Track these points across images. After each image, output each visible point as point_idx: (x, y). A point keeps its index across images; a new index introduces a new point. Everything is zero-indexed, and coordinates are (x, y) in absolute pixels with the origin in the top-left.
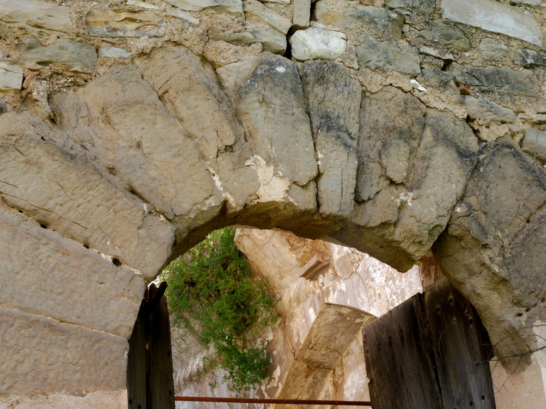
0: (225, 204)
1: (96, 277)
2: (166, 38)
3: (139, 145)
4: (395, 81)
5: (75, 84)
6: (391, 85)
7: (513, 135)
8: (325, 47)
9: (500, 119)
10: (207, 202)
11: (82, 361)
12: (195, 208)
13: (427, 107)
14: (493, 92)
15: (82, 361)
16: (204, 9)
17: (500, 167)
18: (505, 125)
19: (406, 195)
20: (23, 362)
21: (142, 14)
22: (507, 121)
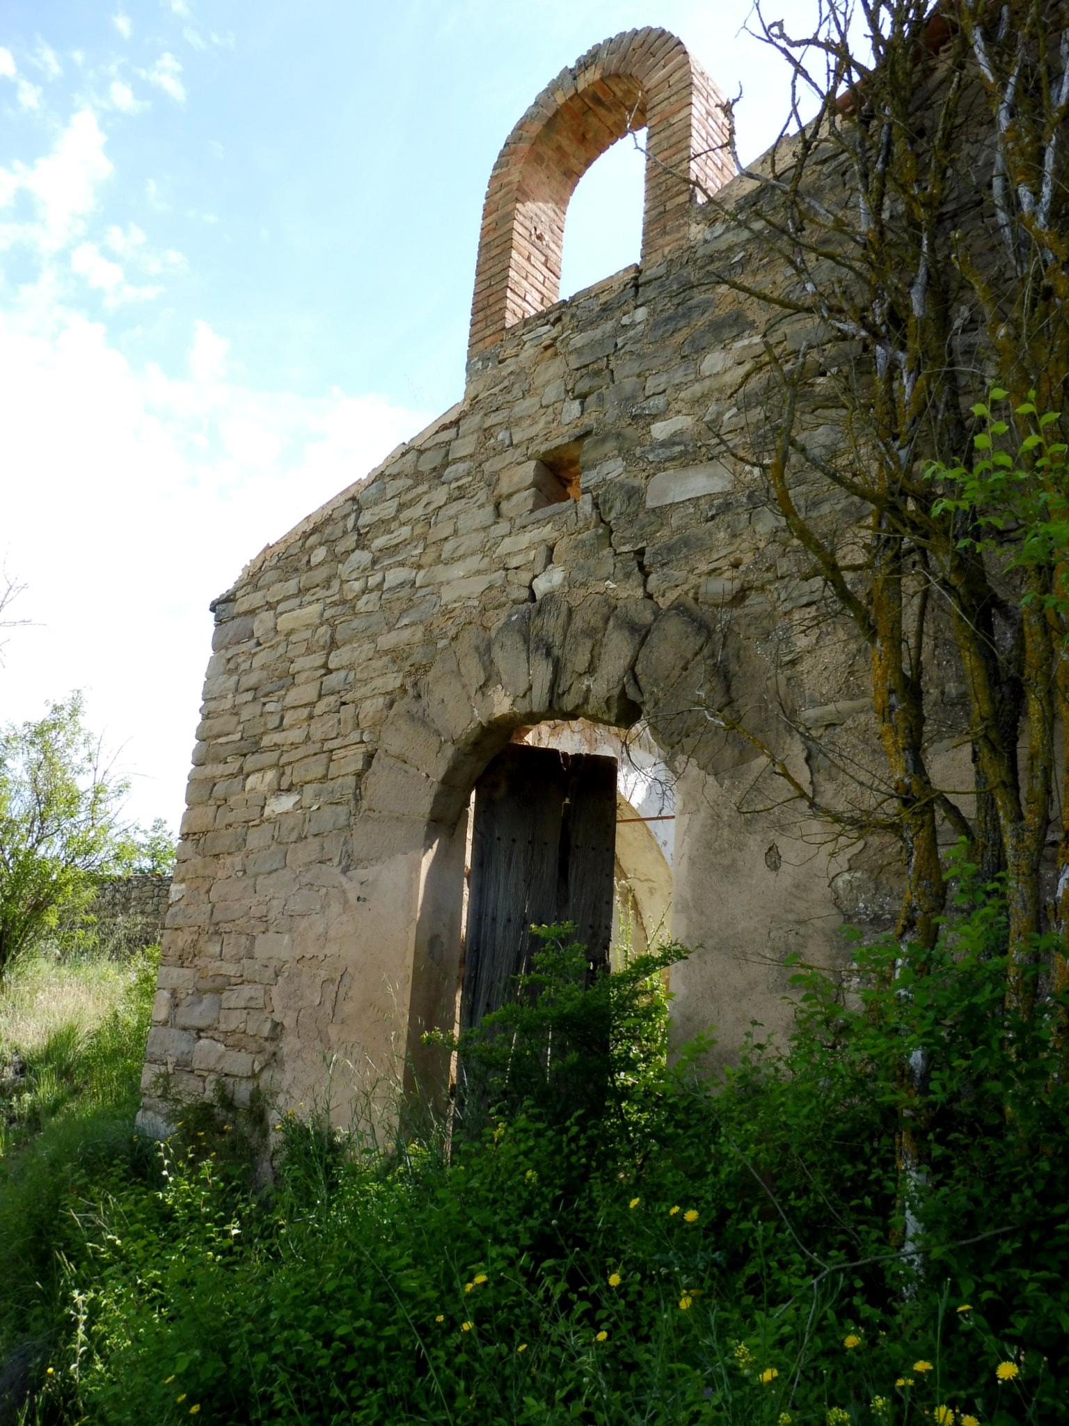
7: (686, 593)
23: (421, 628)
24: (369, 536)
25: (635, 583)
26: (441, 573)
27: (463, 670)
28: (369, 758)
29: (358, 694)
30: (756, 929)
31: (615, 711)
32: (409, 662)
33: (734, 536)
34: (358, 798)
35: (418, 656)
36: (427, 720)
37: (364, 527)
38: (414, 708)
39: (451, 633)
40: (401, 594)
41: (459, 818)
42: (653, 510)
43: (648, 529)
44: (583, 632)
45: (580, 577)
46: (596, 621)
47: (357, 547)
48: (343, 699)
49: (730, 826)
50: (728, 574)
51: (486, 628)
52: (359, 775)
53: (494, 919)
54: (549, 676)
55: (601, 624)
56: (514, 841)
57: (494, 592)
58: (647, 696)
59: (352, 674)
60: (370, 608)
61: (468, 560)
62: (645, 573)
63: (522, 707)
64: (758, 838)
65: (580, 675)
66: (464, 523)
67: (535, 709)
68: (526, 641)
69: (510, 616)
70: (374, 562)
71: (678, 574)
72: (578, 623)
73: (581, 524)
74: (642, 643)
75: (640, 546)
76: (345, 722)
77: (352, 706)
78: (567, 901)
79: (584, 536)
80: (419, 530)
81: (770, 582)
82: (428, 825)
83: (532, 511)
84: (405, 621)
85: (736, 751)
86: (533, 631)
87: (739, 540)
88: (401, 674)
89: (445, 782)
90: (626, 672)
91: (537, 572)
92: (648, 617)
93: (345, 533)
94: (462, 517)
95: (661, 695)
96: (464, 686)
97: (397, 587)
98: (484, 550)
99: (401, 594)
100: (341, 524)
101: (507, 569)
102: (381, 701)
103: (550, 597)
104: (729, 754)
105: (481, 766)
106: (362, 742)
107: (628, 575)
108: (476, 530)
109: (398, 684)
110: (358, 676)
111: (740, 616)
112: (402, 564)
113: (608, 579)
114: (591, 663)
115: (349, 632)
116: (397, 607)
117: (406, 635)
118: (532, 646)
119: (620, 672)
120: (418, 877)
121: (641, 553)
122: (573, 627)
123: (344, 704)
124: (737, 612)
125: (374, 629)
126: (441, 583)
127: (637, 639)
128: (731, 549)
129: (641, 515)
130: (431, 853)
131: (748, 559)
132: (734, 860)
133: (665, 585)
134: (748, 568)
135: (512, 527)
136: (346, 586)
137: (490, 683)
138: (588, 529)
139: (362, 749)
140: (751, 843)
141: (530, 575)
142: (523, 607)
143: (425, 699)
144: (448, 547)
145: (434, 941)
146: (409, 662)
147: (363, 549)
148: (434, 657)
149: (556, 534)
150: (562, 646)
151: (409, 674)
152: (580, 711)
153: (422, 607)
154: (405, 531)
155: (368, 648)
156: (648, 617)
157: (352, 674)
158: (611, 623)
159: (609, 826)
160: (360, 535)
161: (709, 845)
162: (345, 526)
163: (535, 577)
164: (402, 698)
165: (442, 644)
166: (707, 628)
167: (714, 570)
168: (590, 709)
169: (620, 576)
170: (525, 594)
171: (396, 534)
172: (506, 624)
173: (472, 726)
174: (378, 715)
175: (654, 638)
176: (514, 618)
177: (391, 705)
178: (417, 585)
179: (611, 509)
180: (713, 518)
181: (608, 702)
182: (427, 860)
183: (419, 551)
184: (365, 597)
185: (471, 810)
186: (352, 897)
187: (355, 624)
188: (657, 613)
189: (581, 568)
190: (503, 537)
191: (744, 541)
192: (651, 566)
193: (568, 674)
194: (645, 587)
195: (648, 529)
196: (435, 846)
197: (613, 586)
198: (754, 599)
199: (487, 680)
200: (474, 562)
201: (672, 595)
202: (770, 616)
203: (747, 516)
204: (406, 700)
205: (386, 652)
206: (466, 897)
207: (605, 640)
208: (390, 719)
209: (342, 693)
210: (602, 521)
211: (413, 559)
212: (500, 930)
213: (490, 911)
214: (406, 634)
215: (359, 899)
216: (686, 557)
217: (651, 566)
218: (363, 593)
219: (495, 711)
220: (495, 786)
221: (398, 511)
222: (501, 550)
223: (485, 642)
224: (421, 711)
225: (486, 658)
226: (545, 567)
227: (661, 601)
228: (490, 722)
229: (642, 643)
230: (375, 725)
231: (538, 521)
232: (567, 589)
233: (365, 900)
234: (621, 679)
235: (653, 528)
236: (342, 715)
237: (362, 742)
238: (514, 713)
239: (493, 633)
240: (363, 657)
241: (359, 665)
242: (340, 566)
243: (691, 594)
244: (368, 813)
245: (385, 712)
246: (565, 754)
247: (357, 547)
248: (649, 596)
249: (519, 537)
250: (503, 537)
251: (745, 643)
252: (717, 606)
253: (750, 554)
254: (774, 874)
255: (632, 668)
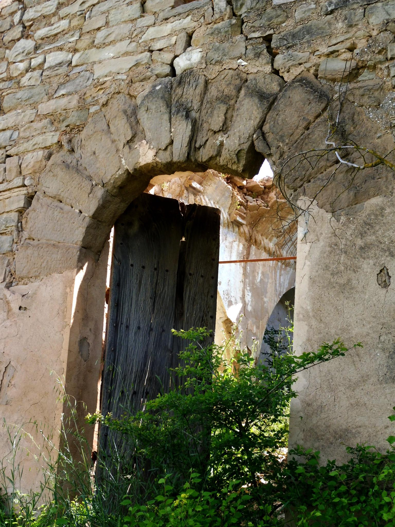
0: (127, 170)
1: (72, 221)
2: (113, 93)
3: (94, 153)
4: (227, 66)
5: (79, 131)
6: (225, 69)
7: (308, 70)
8: (188, 62)
9: (297, 63)
10: (117, 173)
11: (62, 259)
12: (113, 177)
13: (247, 74)
14: (296, 45)
15: (62, 259)
16: (130, 68)
17: (289, 97)
18: (302, 65)
19: (222, 137)
20: (44, 262)
21: (105, 84)
22: (303, 62)
23: (76, 97)
24: (32, 28)
25: (265, 61)
26: (94, 55)
27: (112, 129)
28: (30, 199)
29: (21, 148)
30: (368, 334)
31: (243, 162)
32: (65, 124)
33: (351, 26)
34: (20, 229)
35: (73, 119)
36: (80, 168)
37: (28, 21)
38: (69, 159)
39: (103, 100)
40: (59, 72)
41: (103, 247)
42: (280, 6)
43: (275, 21)
44: (217, 99)
45: (216, 57)
46: (230, 91)
47: (22, 37)
48: (8, 153)
49: (346, 252)
50: (344, 56)
51: (131, 96)
52: (21, 212)
53: (127, 327)
54: (188, 133)
55: (234, 93)
56: (143, 267)
57: (140, 68)
58: (273, 150)
59: (16, 134)
60: (32, 82)
61: (118, 45)
62: (273, 54)
63: (164, 158)
64: (371, 262)
65: (215, 132)
66: (113, 17)
67: (175, 159)
68: (169, 105)
69: (154, 86)
70: (36, 48)
71: (302, 55)
72: (213, 92)
73: (217, 16)
74: (269, 108)
75: (268, 33)
76: (10, 170)
77: (16, 158)
78: (182, 314)
79: (220, 25)
80: (75, 22)
81: (381, 62)
82: (80, 251)
83: (173, 7)
84: (62, 92)
85: (352, 193)
86: (174, 98)
87: (355, 29)
88: (58, 133)
89: (95, 217)
90: (255, 131)
91: (177, 53)
92: (275, 87)
93: (12, 26)
94: (113, 12)
95: (286, 148)
96: (113, 141)
97: (56, 66)
98: (131, 38)
99: (59, 72)
100: (9, 19)
101: (151, 51)
102: (40, 154)
103: (189, 72)
104: (345, 197)
105: (123, 206)
106: (24, 186)
107: (258, 55)
108: (125, 22)
109: (55, 140)
110: (21, 135)
111: (354, 88)
112: (60, 49)
113: (240, 58)
114: (225, 123)
115: (15, 101)
116: (55, 82)
117: (63, 102)
118: (173, 110)
119: (251, 130)
120: (72, 291)
121: (268, 39)
122: (208, 96)
123: (8, 156)
124: (352, 85)
125: (36, 98)
126: (95, 63)
127: (266, 104)
128: (348, 36)
129: (268, 10)
130: (82, 273)
131: (362, 44)
132: (349, 280)
133: (290, 63)
134: (362, 51)
135: (156, 19)
136: (12, 67)
137: (136, 139)
138: (223, 20)
139: (24, 191)
140: (365, 266)
141: (172, 56)
142: (167, 79)
143: (77, 155)
144: (100, 36)
145: (83, 341)
146: (65, 124)
147: (27, 38)
148: (86, 119)
149: (195, 24)
150: (200, 110)
151: (65, 133)
152: (212, 163)
153: (78, 81)
154: (64, 24)
155: (30, 113)
156: (275, 87)
157: (16, 134)
158: (243, 92)
159: (214, 260)
160: (24, 27)
161: (327, 267)
162: (12, 21)
163: (176, 57)
164: (58, 152)
165: (93, 109)
166: (326, 96)
167: (332, 53)
168: (222, 161)
169: (251, 55)
170: (167, 69)
171: (55, 26)
172: (151, 93)
173: (120, 172)
174: (37, 166)
175: (280, 104)
176: (158, 88)
177: (49, 157)
178: (73, 64)
179: (242, 5)
180: (332, 12)
181: (238, 154)
182: (80, 277)
183: (76, 38)
184: (29, 75)
185: (111, 240)
186: (15, 307)
187: (19, 95)
188: (283, 84)
189: (217, 49)
190: (148, 27)
191: (359, 30)
192: (277, 48)
193: (204, 132)
194: (272, 65)
195: (275, 21)
196: (85, 267)
197: (245, 63)
198: (365, 76)
199: (134, 137)
200: (123, 46)
201: (296, 71)
202: (381, 88)
203: (361, 10)
204: (62, 153)
205: (46, 116)
206: (106, 311)
207: (237, 106)
208: (48, 167)
209: (7, 148)
210: (234, 15)
211: (70, 45)
212: (132, 335)
213: (125, 321)
214: (63, 102)
215: (20, 308)
216: (308, 42)
217: (277, 48)
218: (27, 71)
219: (140, 160)
220: (130, 224)
221: (57, 8)
222: (145, 37)
223: (132, 108)
224: (75, 161)
225: (132, 119)
226: (185, 50)
227: (286, 77)
228: (135, 170)
229: (269, 108)
230: (35, 172)
231: (179, 14)
232: (204, 66)
233: (25, 309)
234: (251, 136)
235: (280, 20)
236: (7, 165)
237: (24, 186)
238: (157, 163)
239: (139, 101)
240: (26, 119)
241: (22, 126)
242: (7, 51)
243: (312, 71)
244: (28, 241)
245: (44, 163)
246: (182, 204)
247: (22, 37)
248: (276, 72)
249: (161, 27)
250: (148, 27)
251: (358, 109)
252: (334, 80)
253: (364, 41)
254: (384, 291)
255: (260, 127)
